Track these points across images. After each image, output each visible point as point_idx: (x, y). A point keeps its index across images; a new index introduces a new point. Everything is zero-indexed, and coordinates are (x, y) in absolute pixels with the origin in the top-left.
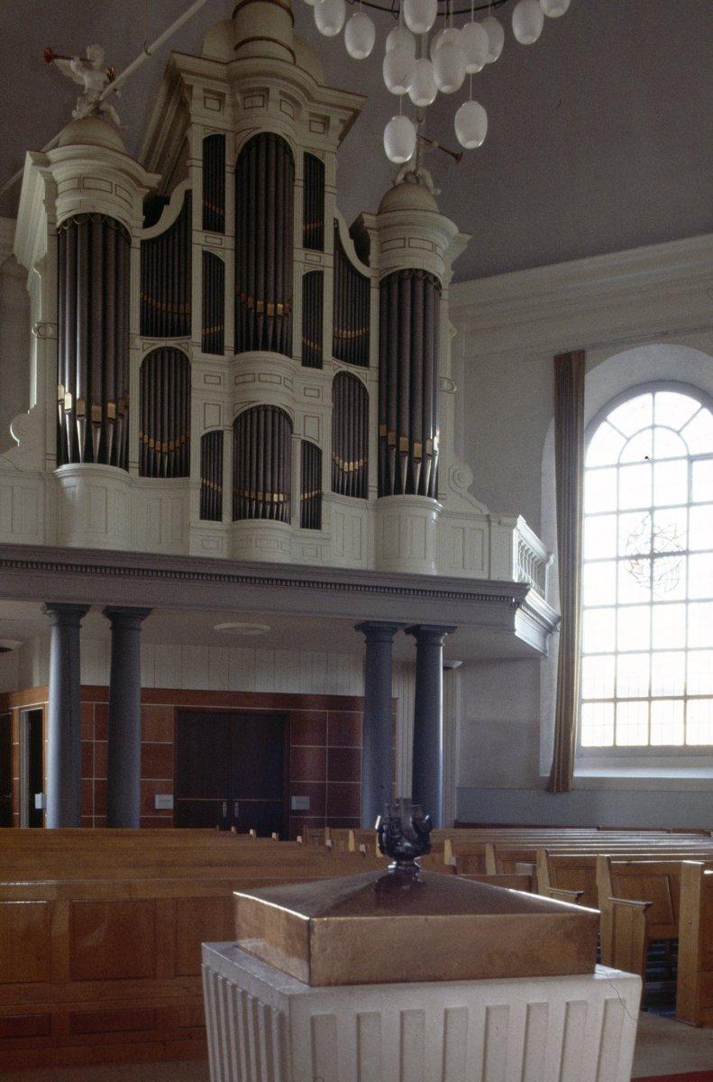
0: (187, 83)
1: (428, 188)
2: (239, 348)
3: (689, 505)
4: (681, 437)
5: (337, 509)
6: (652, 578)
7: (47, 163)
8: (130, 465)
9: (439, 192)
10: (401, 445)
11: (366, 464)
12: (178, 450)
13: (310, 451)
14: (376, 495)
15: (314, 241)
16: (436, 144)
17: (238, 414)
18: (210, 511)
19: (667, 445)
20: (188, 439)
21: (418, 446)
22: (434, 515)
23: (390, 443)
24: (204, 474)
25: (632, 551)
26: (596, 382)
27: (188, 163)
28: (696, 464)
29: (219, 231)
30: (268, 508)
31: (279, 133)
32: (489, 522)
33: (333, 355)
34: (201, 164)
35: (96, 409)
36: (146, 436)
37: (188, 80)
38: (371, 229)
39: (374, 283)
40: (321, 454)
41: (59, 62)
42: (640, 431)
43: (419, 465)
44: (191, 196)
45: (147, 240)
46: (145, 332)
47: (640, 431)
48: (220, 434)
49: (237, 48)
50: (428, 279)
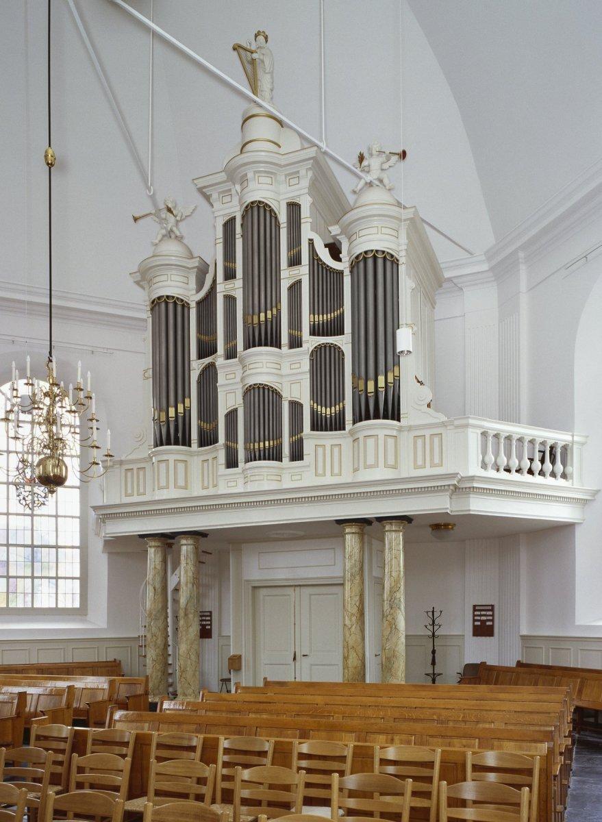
13: (296, 407)
15: (295, 261)
18: (232, 463)
39: (193, 305)
40: (302, 407)
48: (236, 410)
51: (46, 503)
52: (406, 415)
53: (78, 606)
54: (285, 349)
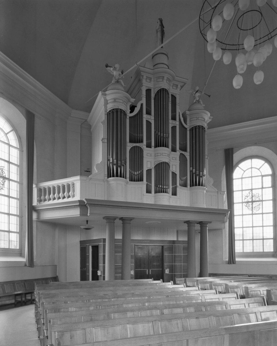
0: (142, 74)
1: (201, 105)
2: (156, 147)
3: (262, 188)
4: (260, 171)
5: (180, 190)
6: (252, 207)
7: (106, 95)
8: (127, 178)
9: (204, 105)
10: (118, 164)
11: (187, 178)
12: (140, 174)
14: (189, 186)
15: (174, 118)
16: (203, 93)
17: (156, 164)
18: (148, 191)
19: (256, 172)
20: (142, 171)
21: (201, 173)
22: (205, 191)
23: (193, 172)
24: (147, 181)
25: (246, 200)
26: (236, 156)
27: (142, 96)
28: (264, 178)
29: (150, 115)
30: (165, 190)
31: (166, 88)
32: (218, 193)
33: (179, 149)
34: (145, 96)
35: (119, 162)
36: (131, 170)
37: (142, 73)
38: (188, 115)
39: (188, 129)
41: (108, 68)
42: (248, 169)
43: (202, 178)
44: (143, 105)
45: (131, 117)
46: (131, 141)
47: (248, 169)
48: (151, 169)
49: (154, 66)
50: (203, 128)
51: (3, 188)
52: (105, 175)
53: (272, 251)
54: (153, 148)
